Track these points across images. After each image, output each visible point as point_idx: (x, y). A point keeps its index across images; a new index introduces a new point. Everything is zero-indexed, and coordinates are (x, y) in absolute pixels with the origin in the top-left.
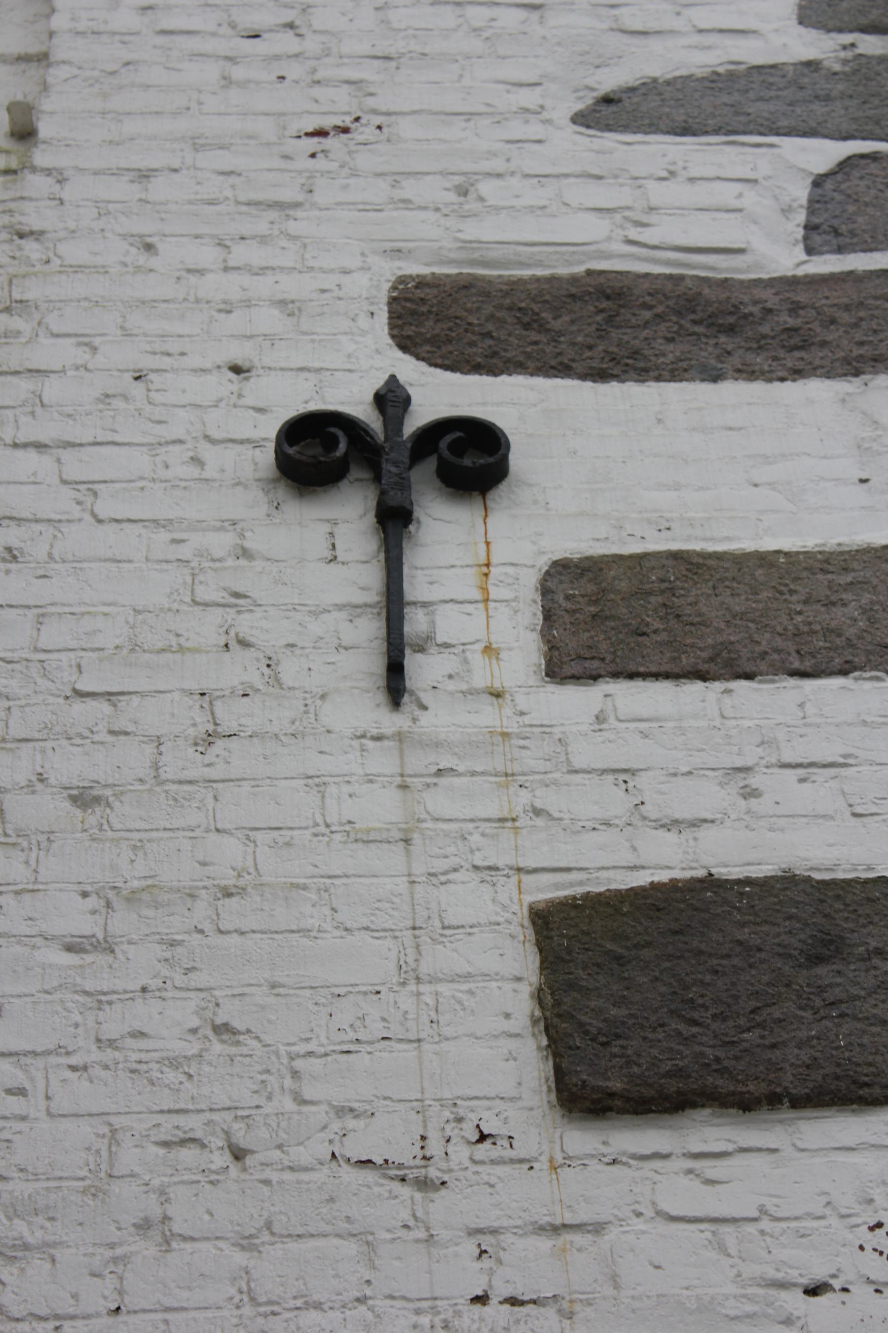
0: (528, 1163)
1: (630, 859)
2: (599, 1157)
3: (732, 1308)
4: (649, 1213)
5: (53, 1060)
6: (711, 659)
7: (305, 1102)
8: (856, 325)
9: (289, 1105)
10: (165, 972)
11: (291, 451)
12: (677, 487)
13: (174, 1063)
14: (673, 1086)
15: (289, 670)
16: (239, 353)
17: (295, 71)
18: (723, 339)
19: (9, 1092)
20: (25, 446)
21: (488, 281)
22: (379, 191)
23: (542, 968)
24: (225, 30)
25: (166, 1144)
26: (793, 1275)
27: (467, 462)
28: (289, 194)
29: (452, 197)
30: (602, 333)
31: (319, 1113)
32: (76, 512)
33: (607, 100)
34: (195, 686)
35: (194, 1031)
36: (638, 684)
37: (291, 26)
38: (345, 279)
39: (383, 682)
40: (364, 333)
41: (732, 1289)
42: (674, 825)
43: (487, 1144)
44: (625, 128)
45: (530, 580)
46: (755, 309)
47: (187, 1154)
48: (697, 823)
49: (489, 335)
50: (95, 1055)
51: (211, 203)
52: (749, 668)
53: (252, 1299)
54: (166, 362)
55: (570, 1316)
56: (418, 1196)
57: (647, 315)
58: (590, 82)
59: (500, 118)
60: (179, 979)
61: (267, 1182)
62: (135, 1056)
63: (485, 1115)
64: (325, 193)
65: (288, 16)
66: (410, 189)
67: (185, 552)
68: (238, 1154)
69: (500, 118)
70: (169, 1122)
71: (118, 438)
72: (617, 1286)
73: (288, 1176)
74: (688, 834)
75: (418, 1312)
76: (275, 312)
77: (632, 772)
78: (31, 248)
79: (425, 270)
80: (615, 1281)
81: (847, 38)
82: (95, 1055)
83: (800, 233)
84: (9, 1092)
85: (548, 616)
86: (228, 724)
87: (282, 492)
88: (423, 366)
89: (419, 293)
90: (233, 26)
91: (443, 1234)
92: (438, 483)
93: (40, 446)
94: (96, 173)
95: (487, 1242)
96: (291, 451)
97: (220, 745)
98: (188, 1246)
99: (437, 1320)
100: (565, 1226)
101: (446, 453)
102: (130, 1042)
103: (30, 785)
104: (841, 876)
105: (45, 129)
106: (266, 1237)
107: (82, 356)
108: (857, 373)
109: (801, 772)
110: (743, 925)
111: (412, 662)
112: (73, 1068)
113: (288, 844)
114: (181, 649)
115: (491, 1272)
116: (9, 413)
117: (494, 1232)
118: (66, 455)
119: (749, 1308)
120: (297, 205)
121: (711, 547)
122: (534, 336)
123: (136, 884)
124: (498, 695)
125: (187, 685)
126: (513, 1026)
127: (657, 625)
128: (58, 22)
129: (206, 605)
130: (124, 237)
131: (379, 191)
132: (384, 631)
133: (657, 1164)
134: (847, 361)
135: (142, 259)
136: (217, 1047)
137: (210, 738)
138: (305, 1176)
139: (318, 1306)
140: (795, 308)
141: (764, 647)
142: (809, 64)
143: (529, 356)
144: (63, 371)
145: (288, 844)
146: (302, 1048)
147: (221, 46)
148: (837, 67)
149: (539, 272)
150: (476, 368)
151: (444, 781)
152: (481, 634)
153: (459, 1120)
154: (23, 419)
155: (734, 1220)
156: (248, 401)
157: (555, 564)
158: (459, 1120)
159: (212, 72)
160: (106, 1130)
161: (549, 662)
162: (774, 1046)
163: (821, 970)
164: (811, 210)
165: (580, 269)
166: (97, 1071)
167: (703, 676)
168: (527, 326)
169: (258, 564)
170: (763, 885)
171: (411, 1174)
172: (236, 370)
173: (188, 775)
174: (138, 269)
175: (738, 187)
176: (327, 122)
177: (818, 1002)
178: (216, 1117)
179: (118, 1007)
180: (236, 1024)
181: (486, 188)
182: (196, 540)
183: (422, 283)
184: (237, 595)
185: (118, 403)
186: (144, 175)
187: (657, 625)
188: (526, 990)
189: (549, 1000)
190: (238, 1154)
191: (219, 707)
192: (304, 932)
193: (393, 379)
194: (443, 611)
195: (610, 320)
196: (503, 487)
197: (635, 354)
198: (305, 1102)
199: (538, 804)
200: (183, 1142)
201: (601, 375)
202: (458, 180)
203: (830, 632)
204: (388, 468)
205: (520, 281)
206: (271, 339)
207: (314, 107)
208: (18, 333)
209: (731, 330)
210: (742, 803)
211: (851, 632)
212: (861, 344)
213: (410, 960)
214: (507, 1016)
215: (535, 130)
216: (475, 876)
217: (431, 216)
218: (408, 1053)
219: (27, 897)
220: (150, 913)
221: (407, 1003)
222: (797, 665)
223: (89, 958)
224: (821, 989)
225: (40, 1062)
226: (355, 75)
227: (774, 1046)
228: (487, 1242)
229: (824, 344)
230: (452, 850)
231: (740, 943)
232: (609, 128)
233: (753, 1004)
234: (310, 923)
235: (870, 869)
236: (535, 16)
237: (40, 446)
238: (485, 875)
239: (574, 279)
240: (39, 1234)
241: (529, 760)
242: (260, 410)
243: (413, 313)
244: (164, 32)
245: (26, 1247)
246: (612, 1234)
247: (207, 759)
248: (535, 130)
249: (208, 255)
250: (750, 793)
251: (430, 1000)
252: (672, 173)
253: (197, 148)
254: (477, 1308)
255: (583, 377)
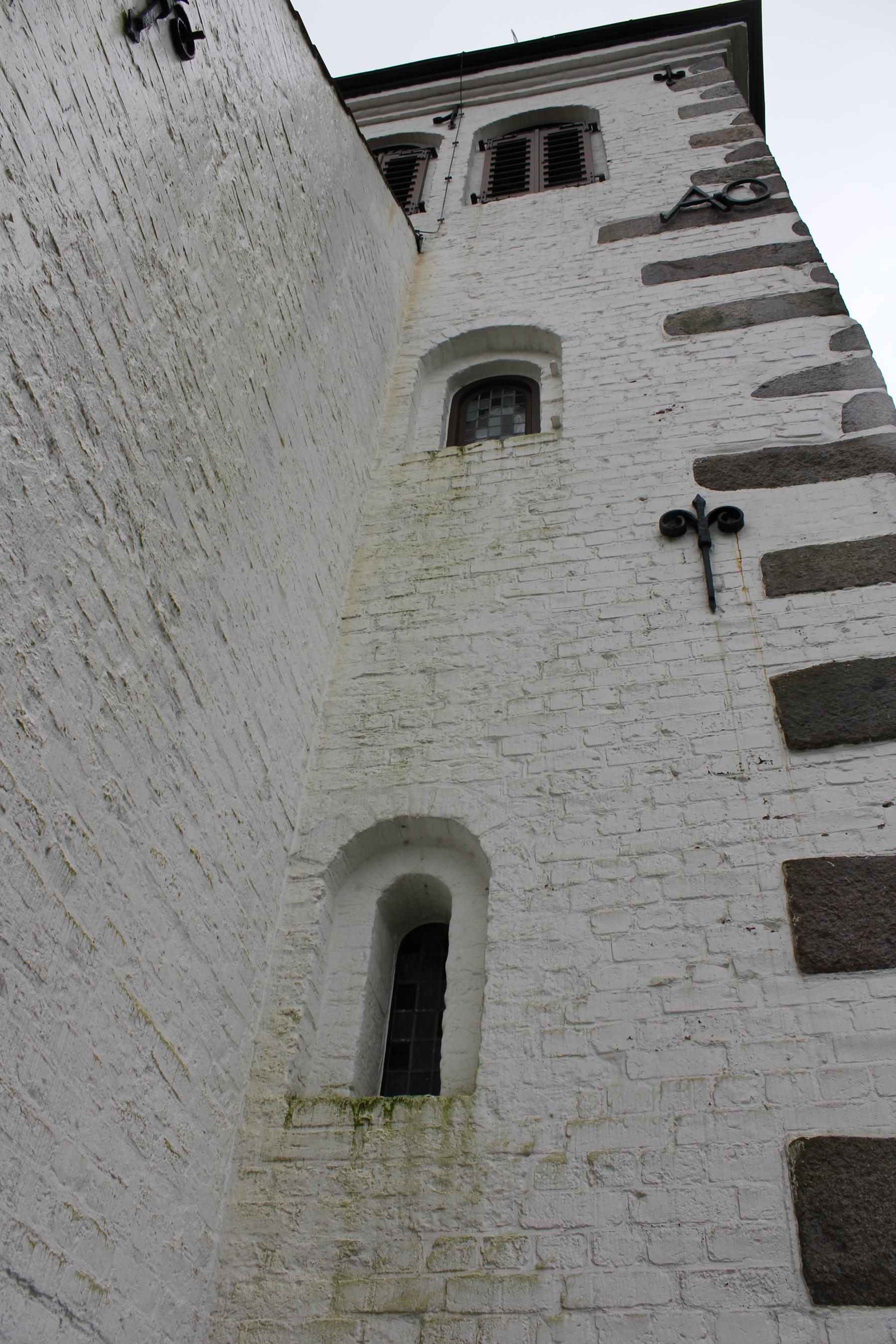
0: (778, 769)
1: (805, 659)
2: (804, 765)
3: (858, 814)
4: (824, 783)
5: (607, 747)
6: (826, 584)
7: (697, 754)
8: (865, 456)
9: (691, 756)
10: (642, 713)
11: (665, 526)
12: (806, 523)
13: (649, 745)
14: (829, 738)
15: (673, 603)
16: (642, 493)
17: (650, 392)
18: (816, 467)
19: (594, 759)
20: (572, 535)
21: (728, 457)
22: (685, 430)
23: (777, 699)
24: (623, 381)
25: (649, 773)
26: (878, 800)
27: (729, 522)
28: (653, 435)
29: (712, 428)
30: (772, 470)
31: (702, 758)
32: (592, 556)
33: (763, 387)
34: (641, 613)
35: (655, 733)
36: (800, 595)
37: (646, 376)
38: (677, 462)
39: (708, 604)
40: (686, 481)
41: (856, 807)
42: (819, 645)
43: (763, 764)
44: (771, 396)
45: (757, 562)
46: (827, 455)
47: (658, 776)
48: (827, 643)
49: (731, 476)
50: (621, 744)
51: (626, 442)
52: (841, 585)
53: (686, 823)
54: (617, 500)
55: (799, 821)
56: (741, 784)
57: (788, 462)
58: (756, 381)
59: (726, 398)
60: (648, 716)
61: (686, 783)
62: (635, 743)
63: (761, 754)
64: (665, 434)
65: (645, 373)
66: (696, 428)
67: (632, 566)
68: (675, 774)
69: (726, 398)
70: (650, 765)
71: (603, 528)
72: (815, 810)
73: (694, 780)
74: (824, 647)
75: (744, 824)
76: (653, 477)
77: (802, 627)
78: (565, 465)
79: (705, 456)
80: (814, 807)
81: (849, 353)
82: (621, 744)
83: (840, 425)
84: (594, 759)
85: (764, 574)
86: (654, 624)
87: (663, 541)
88: (708, 490)
89: (704, 464)
90: (626, 379)
91: (750, 796)
92: (719, 531)
93: (577, 535)
94: (584, 437)
95: (767, 798)
96: (665, 526)
97: (652, 632)
98: (661, 807)
99: (752, 826)
100: (794, 790)
101: (721, 520)
102: (633, 739)
103: (588, 653)
104: (882, 657)
105: (565, 424)
106: (688, 802)
107: (588, 501)
108: (868, 474)
109: (864, 621)
110: (848, 678)
111: (717, 596)
112: (615, 749)
113: (681, 665)
114: (635, 600)
115: (769, 808)
116: (565, 524)
117: (769, 794)
118: (586, 536)
119: (863, 813)
120: (656, 439)
121: (821, 543)
122: (747, 474)
123: (629, 684)
124: (750, 604)
125: (638, 613)
126: (768, 721)
127: (805, 573)
128: (564, 387)
129: (642, 583)
130: (597, 458)
131: (685, 430)
132: (706, 586)
133: (825, 766)
134: (863, 470)
135: (604, 465)
136: (664, 738)
137: (648, 630)
138: (699, 780)
139: (709, 824)
140: (842, 453)
141: (845, 577)
142: (836, 364)
143: (746, 482)
144: (582, 507)
145: (681, 665)
146: (694, 736)
147: (623, 387)
148: (847, 364)
149: (746, 451)
150: (728, 489)
151: (733, 637)
152: (741, 583)
153: (752, 756)
154: (570, 526)
155: (855, 783)
156: (648, 510)
157: (765, 555)
158: (752, 756)
159: (621, 396)
160: (628, 769)
161: (767, 591)
162: (864, 720)
163: (879, 692)
164: (843, 417)
165: (761, 448)
166: (623, 750)
167: (824, 590)
168: (744, 471)
169: (658, 567)
170: (854, 663)
171: (737, 776)
172: (642, 499)
173: (643, 644)
174: (603, 468)
175: (816, 411)
176: (664, 408)
177: (879, 703)
178: (666, 762)
179: (627, 727)
180: (669, 729)
181: (723, 424)
182: (635, 561)
183: (704, 460)
184: (652, 579)
185: (602, 516)
186: (601, 435)
187: (805, 573)
188: (771, 708)
189: (780, 711)
190: (675, 774)
191: (650, 619)
192: (690, 695)
193: (698, 496)
194: (726, 576)
195: (774, 465)
196: (743, 529)
197: (785, 476)
198: (697, 754)
199: (769, 642)
200: (656, 772)
201: (773, 486)
202: (713, 422)
203: (868, 569)
204: (701, 528)
205: (740, 455)
206: (653, 487)
207: (658, 403)
208: (564, 496)
209: (819, 464)
210: (843, 635)
211: (876, 568)
212: (868, 463)
213: (729, 701)
214: (766, 718)
215: (738, 401)
216: (749, 670)
217: (704, 436)
218: (732, 734)
219: (591, 692)
220: (635, 693)
221: (729, 717)
222: (858, 582)
223: (615, 711)
224: (879, 698)
225: (603, 748)
226: (671, 390)
227: (864, 720)
228: (767, 798)
229: (854, 465)
230: (739, 661)
231: (79, 961)
232: (765, 397)
233: (855, 706)
234: (692, 692)
235: (893, 653)
236: (733, 360)
237: (577, 535)
238: (752, 669)
239: (759, 452)
240: (610, 806)
241: (764, 627)
242: (652, 513)
243: (703, 471)
244: (602, 385)
245: (606, 811)
246: (811, 791)
247: (649, 637)
248: (738, 401)
249: (627, 460)
250: (846, 631)
251: (737, 715)
252: (791, 410)
253: (618, 423)
254: (766, 821)
255: (767, 487)
